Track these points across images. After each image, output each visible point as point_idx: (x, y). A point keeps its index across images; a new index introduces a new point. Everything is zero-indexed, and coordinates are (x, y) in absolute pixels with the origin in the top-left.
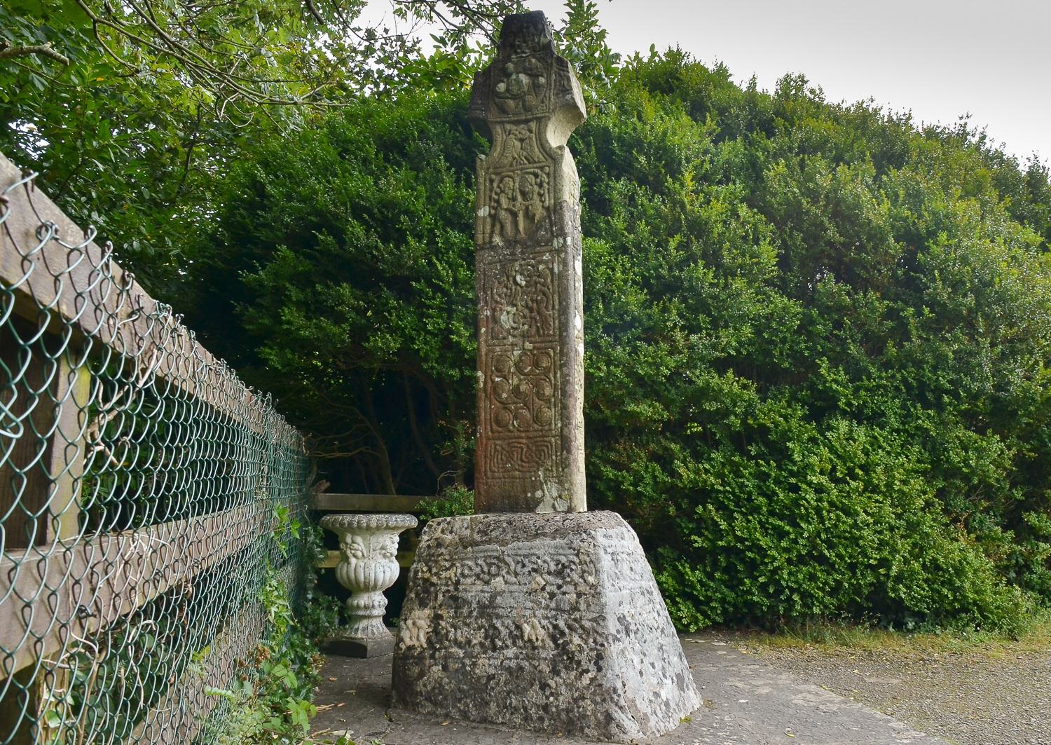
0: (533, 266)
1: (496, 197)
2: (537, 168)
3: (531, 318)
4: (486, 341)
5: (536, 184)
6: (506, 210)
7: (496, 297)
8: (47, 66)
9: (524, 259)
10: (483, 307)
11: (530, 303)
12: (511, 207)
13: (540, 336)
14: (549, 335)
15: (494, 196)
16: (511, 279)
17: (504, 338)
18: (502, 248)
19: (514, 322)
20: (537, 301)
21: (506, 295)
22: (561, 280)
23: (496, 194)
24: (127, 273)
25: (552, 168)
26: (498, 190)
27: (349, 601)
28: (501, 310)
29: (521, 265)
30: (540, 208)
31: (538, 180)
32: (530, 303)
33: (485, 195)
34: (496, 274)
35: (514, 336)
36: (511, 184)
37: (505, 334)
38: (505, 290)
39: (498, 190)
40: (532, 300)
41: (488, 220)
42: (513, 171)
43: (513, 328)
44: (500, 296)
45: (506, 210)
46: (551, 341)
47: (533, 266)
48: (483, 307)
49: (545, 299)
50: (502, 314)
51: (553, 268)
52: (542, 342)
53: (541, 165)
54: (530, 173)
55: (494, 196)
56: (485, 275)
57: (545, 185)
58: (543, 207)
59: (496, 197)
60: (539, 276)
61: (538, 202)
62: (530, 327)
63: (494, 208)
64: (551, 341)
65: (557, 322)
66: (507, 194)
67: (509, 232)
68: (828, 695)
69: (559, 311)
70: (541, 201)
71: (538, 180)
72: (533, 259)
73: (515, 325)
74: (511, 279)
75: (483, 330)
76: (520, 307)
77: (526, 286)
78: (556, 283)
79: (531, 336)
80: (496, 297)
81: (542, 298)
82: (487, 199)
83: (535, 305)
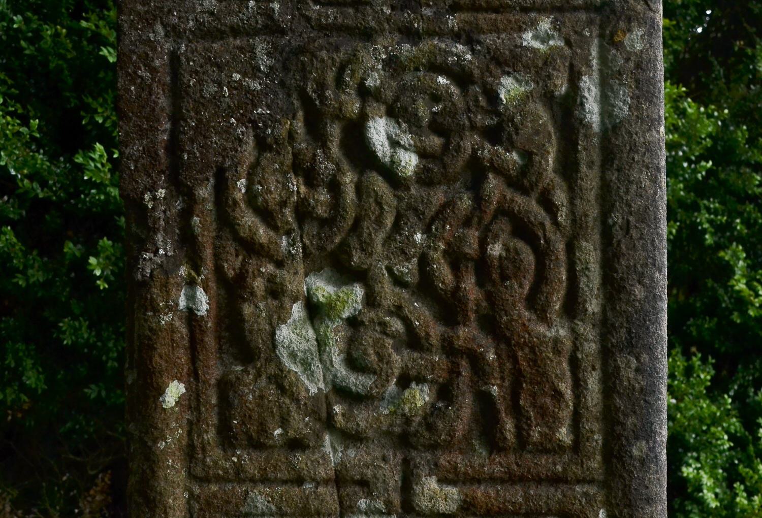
0: (462, 77)
3: (449, 348)
4: (191, 453)
7: (248, 220)
8: (55, 165)
9: (410, 35)
10: (168, 269)
11: (444, 272)
13: (494, 444)
14: (551, 448)
16: (335, 131)
17: (296, 444)
19: (352, 363)
20: (482, 265)
21: (303, 212)
24: (725, 425)
27: (584, 122)
28: (276, 291)
29: (393, 64)
32: (444, 272)
34: (254, 99)
35: (351, 437)
37: (301, 424)
38: (297, 185)
40: (455, 259)
43: (342, 392)
44: (267, 216)
46: (556, 480)
47: (462, 77)
48: (168, 269)
49: (528, 257)
50: (282, 316)
51: (574, 95)
52: (511, 479)
56: (177, 91)
60: (494, 135)
62: (445, 393)
64: (556, 480)
65: (593, 382)
69: (605, 327)
72: (468, 37)
73: (356, 382)
74: (335, 131)
75: (174, 391)
76: (388, 293)
77: (425, 178)
78: (590, 179)
79: (448, 446)
80: (248, 220)
81: (511, 256)
83: (469, 284)
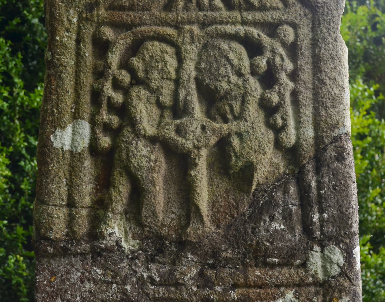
1: (118, 97)
2: (255, 24)
5: (253, 73)
6: (153, 140)
12: (170, 132)
15: (108, 90)
18: (133, 257)
22: (346, 176)
23: (117, 85)
25: (305, 31)
26: (125, 77)
30: (270, 149)
31: (262, 62)
33: (78, 84)
36: (172, 63)
39: (125, 77)
41: (88, 163)
42: (177, 26)
45: (153, 140)
53: (269, 16)
54: (235, 37)
55: (108, 90)
57: (284, 78)
58: (278, 144)
59: (118, 97)
61: (261, 128)
63: (107, 128)
66: (156, 92)
67: (160, 207)
68: (162, 205)
70: (271, 125)
71: (262, 62)
82: (86, 98)
